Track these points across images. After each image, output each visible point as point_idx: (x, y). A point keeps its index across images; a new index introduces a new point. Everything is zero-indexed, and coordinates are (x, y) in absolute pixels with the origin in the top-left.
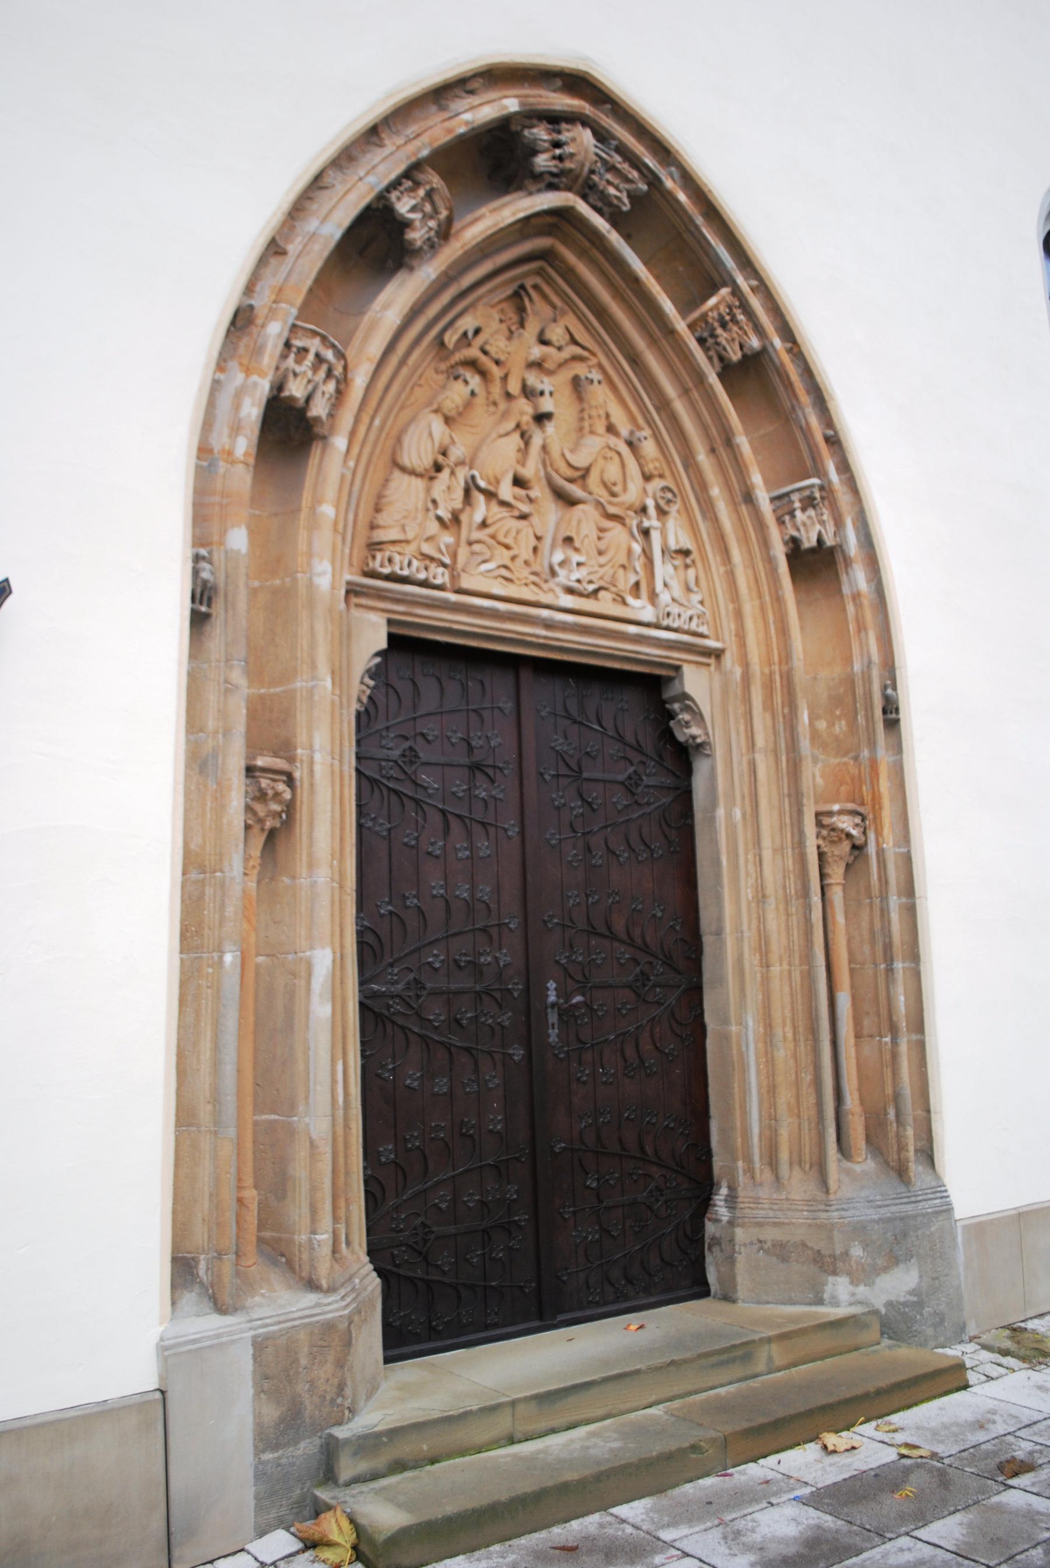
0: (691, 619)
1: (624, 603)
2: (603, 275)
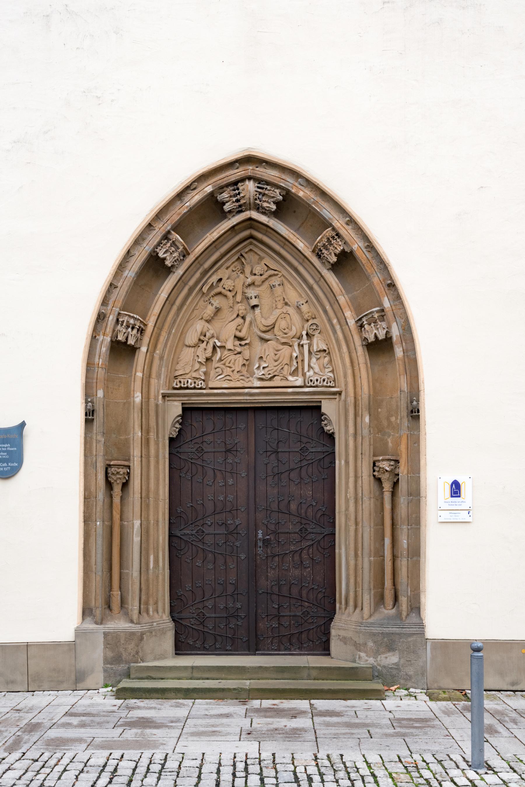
0: (324, 380)
1: (287, 379)
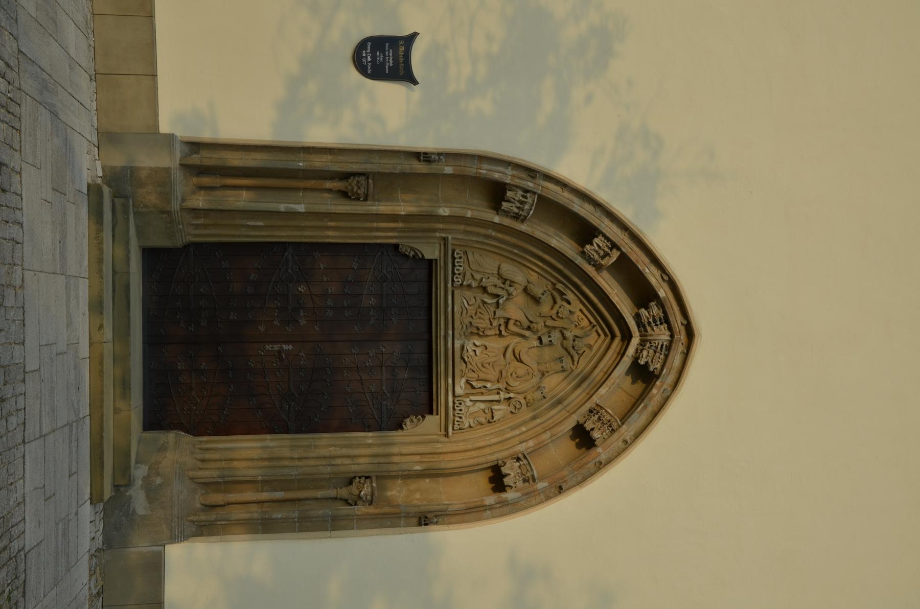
0: (461, 418)
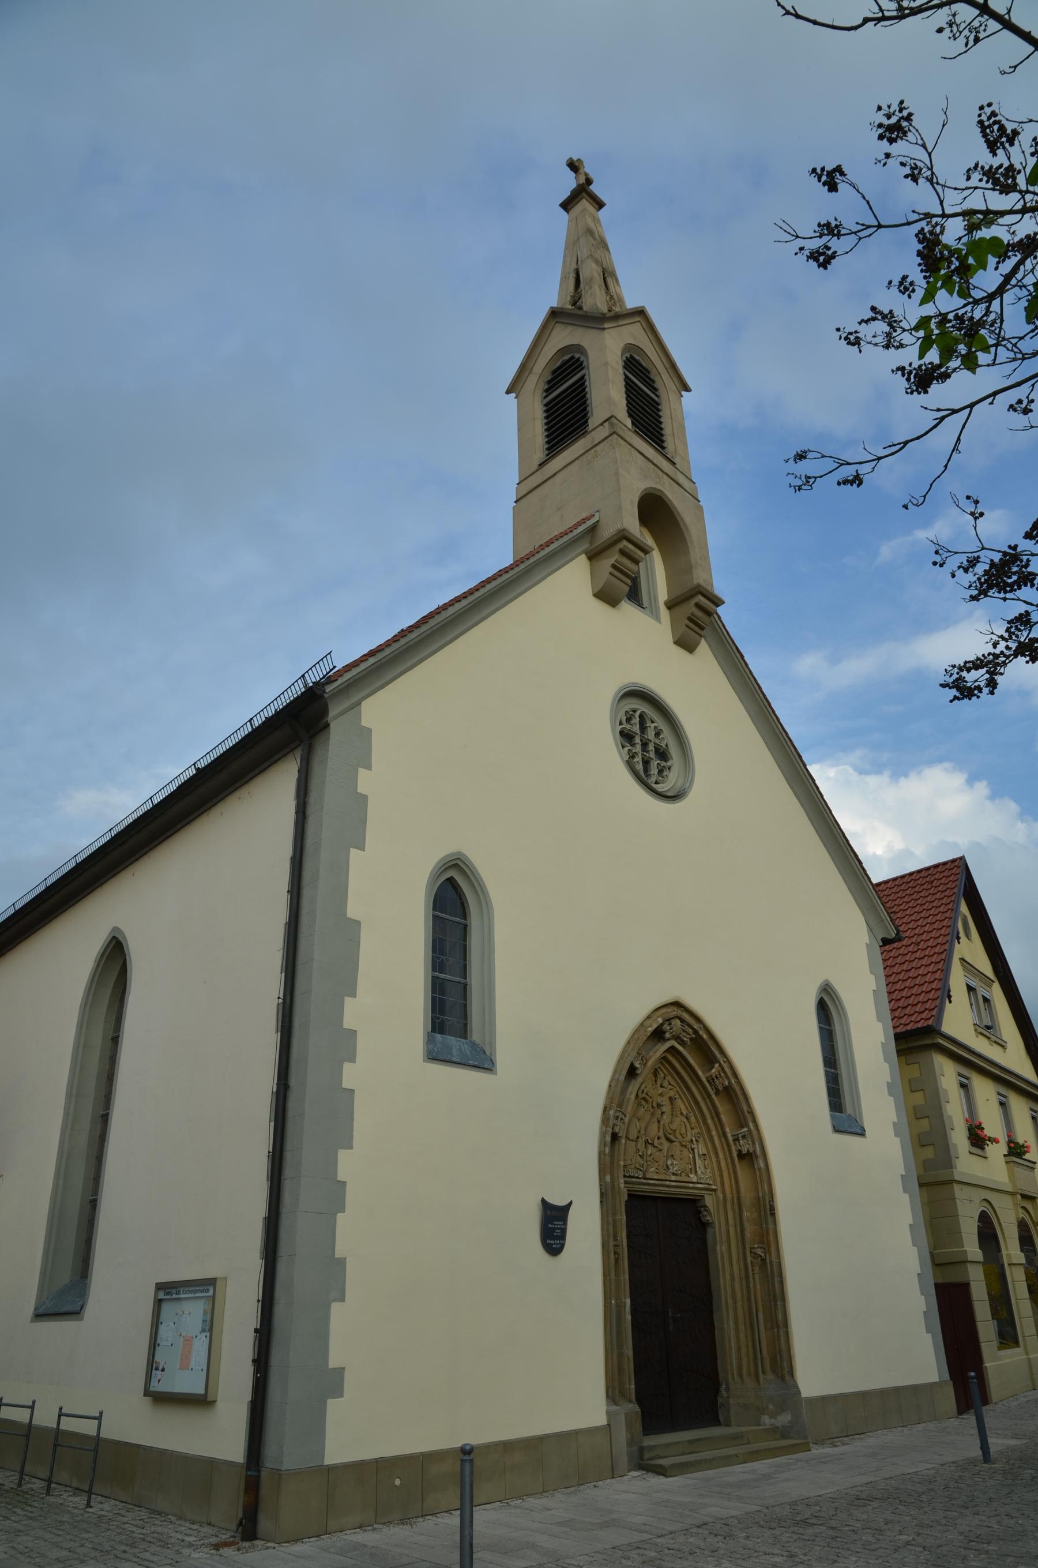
2: (677, 1059)
